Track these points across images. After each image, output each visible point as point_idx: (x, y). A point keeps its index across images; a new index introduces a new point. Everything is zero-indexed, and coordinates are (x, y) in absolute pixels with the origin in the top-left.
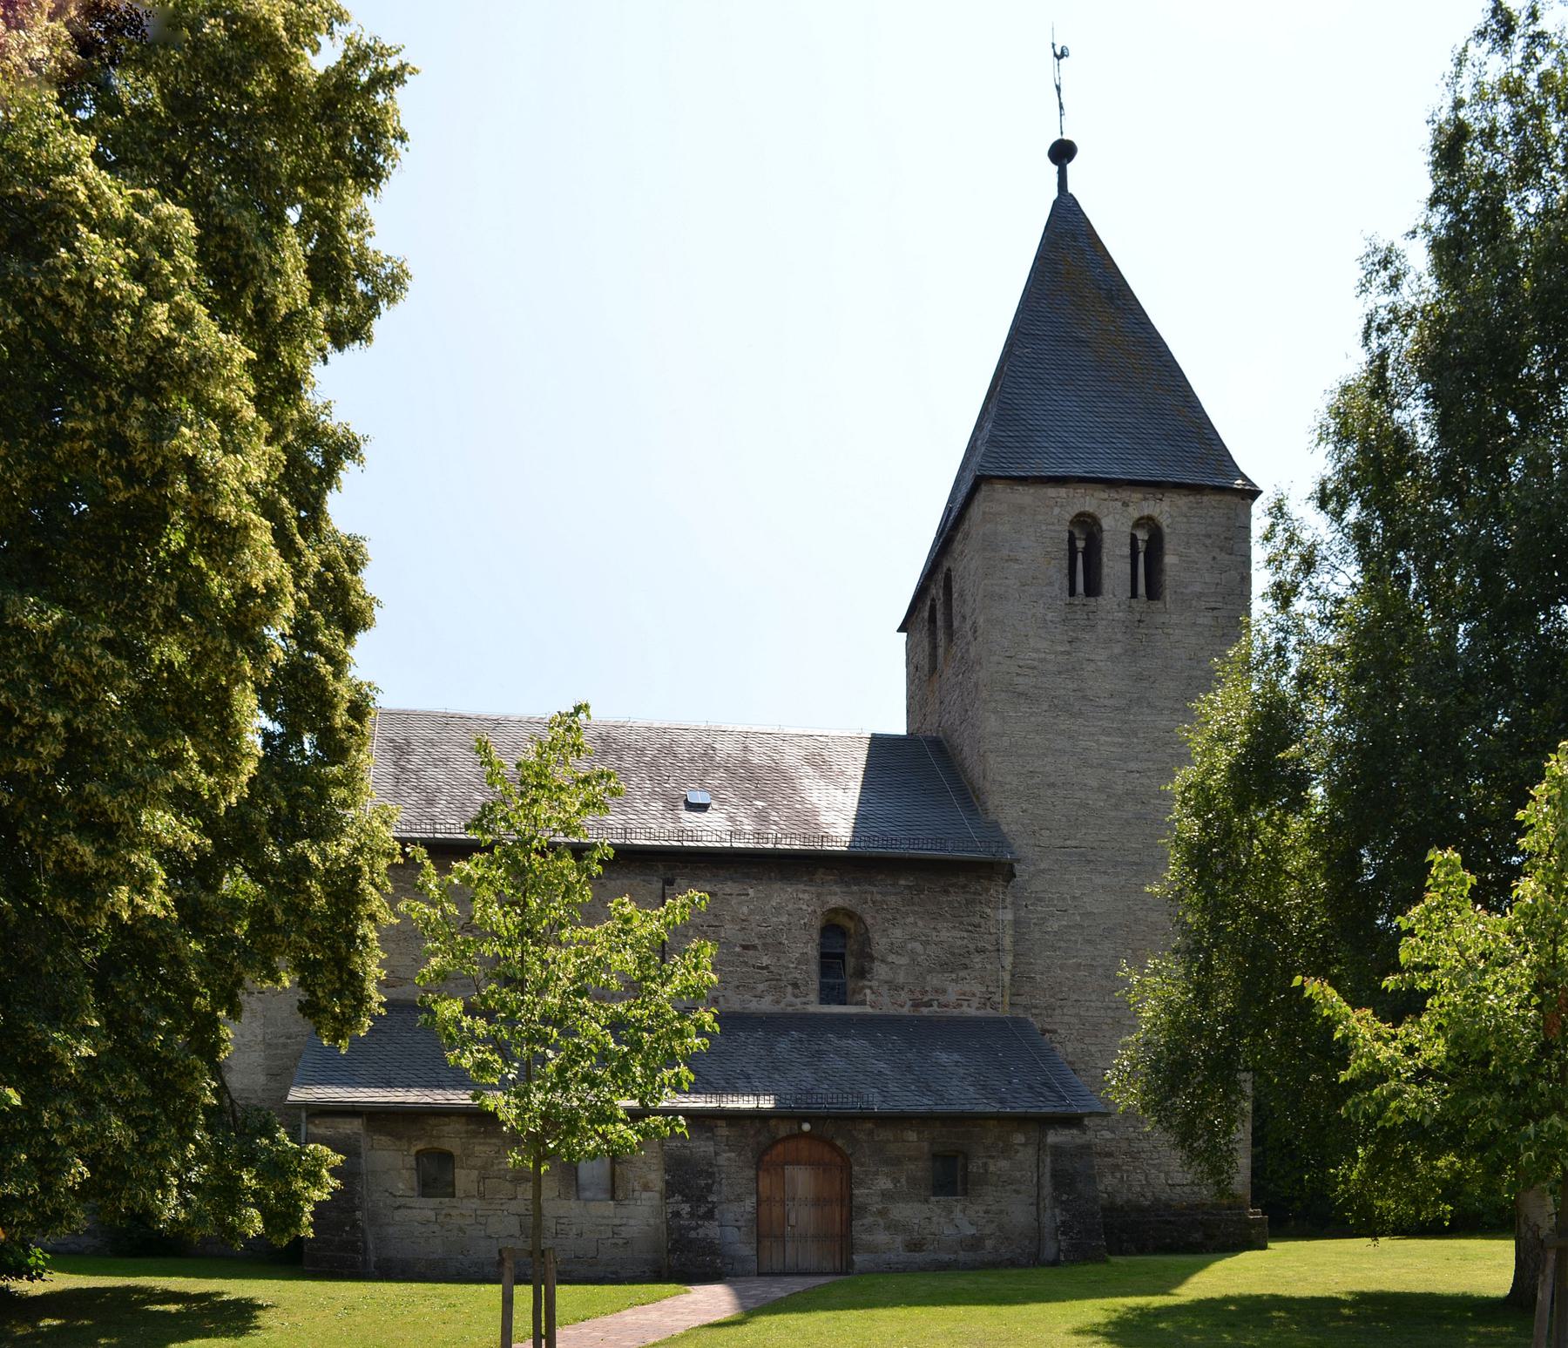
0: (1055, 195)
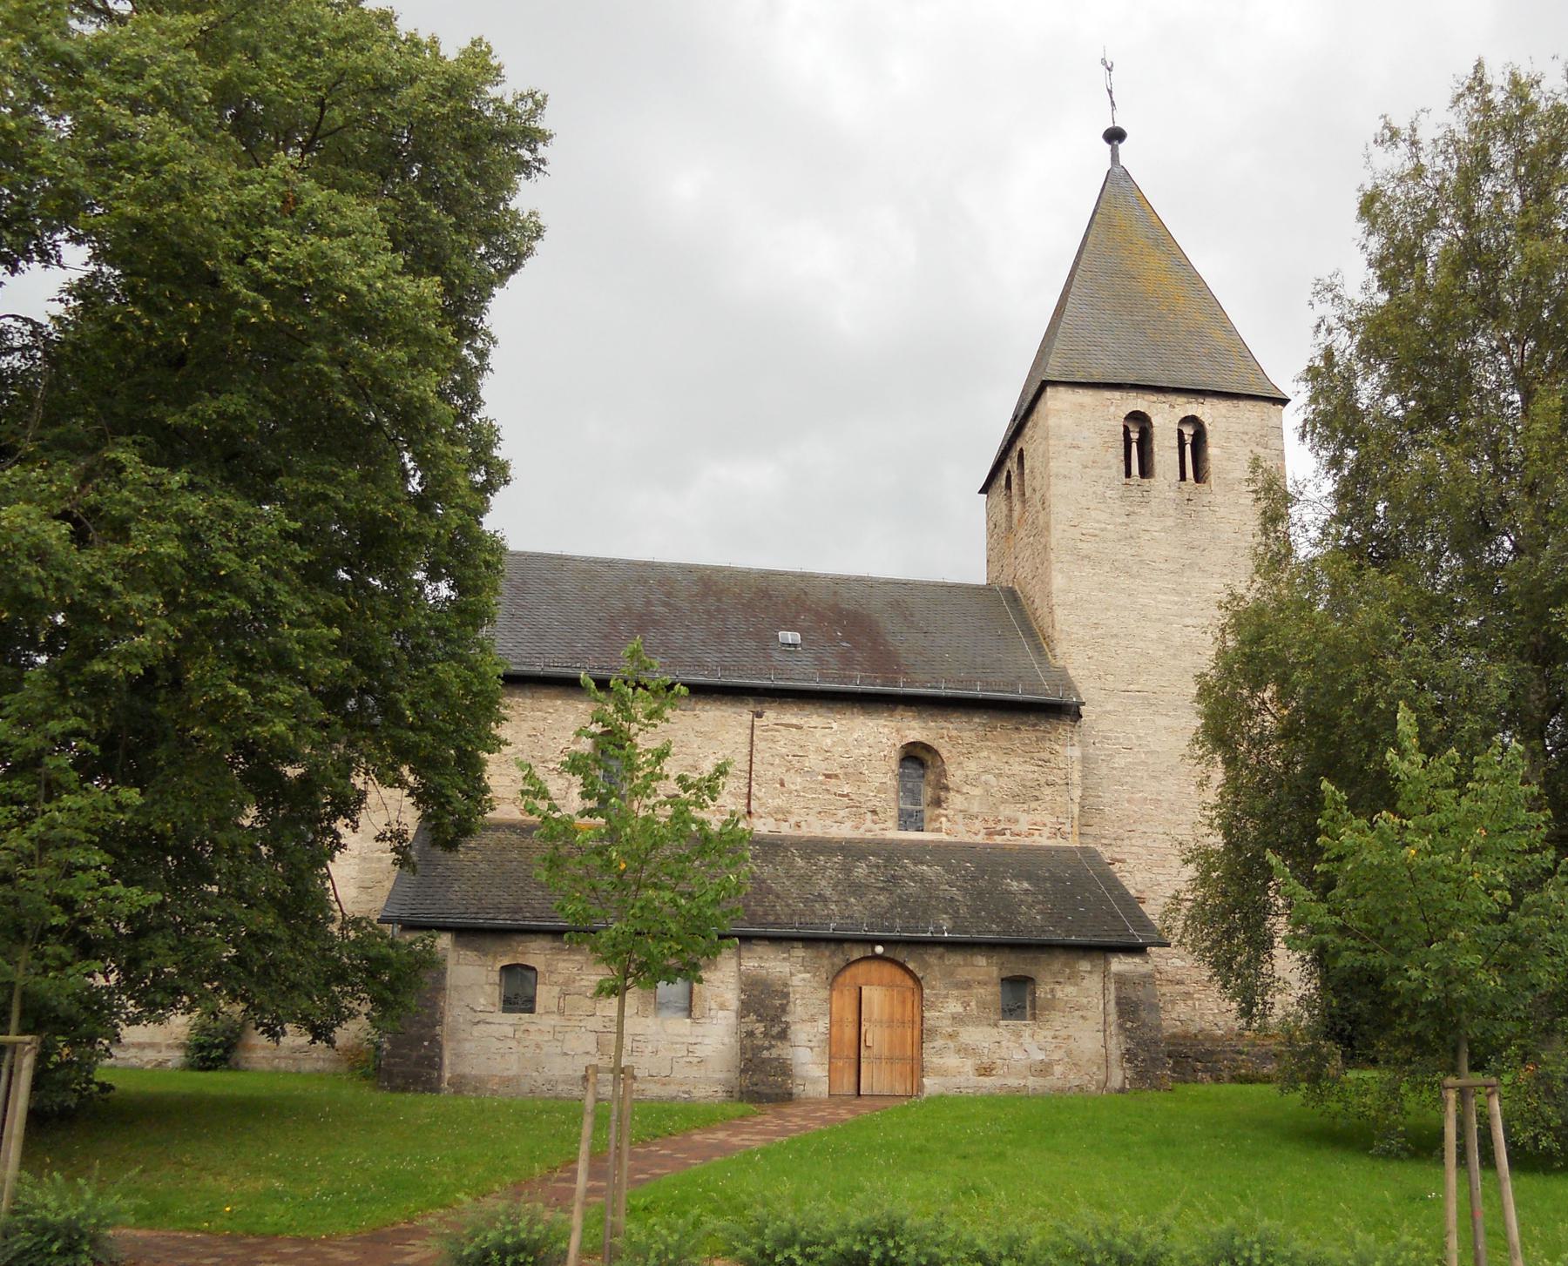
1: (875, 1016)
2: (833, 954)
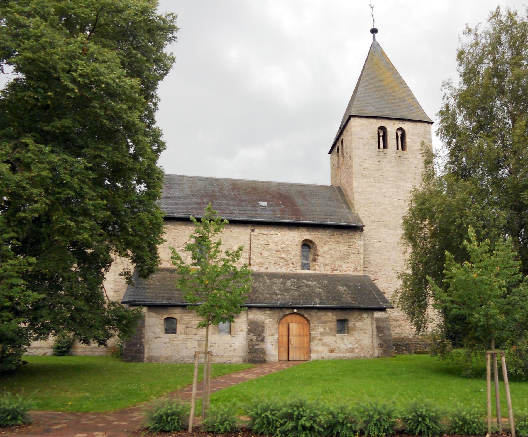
2: (279, 312)
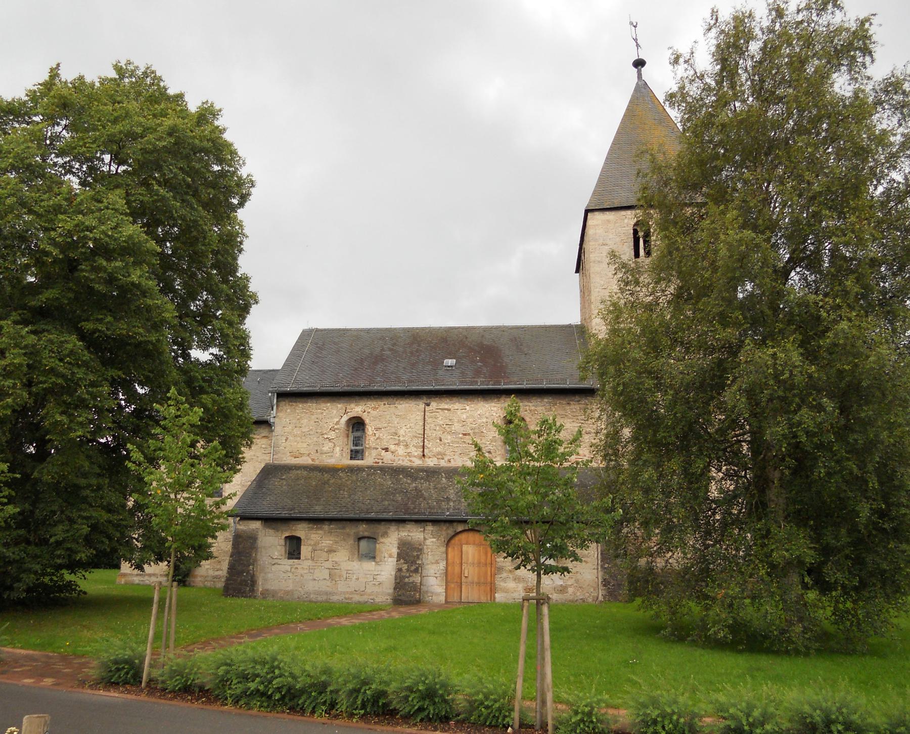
0: (636, 80)
1: (470, 560)
2: (448, 528)
